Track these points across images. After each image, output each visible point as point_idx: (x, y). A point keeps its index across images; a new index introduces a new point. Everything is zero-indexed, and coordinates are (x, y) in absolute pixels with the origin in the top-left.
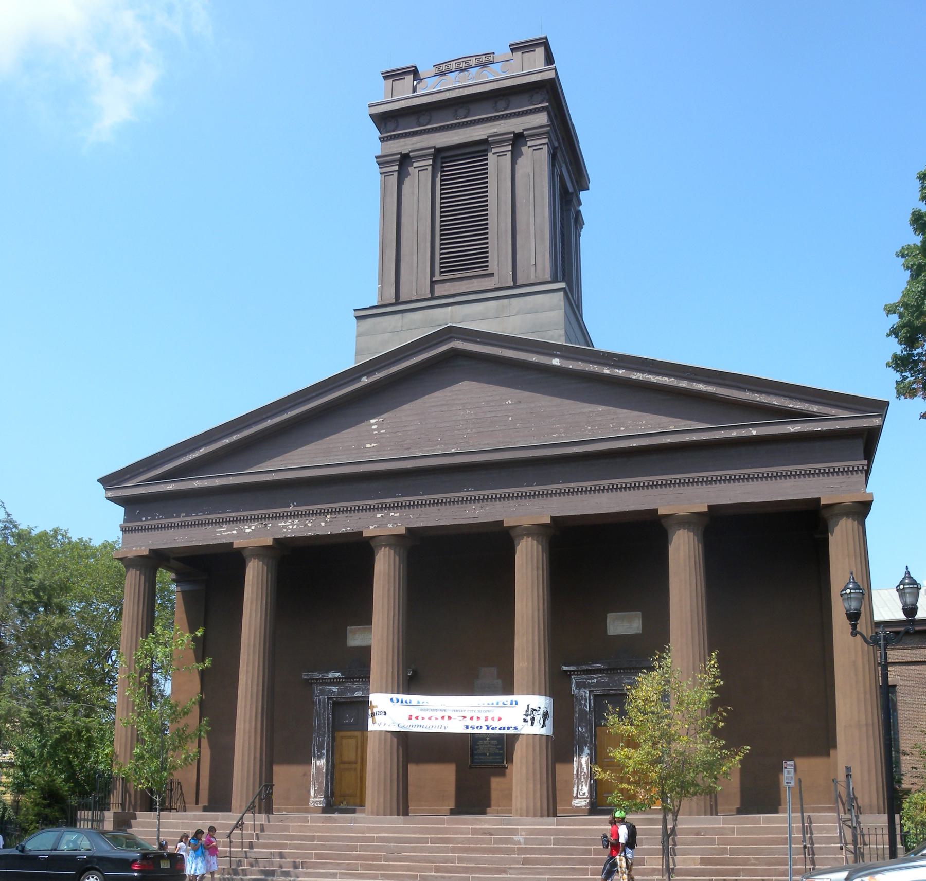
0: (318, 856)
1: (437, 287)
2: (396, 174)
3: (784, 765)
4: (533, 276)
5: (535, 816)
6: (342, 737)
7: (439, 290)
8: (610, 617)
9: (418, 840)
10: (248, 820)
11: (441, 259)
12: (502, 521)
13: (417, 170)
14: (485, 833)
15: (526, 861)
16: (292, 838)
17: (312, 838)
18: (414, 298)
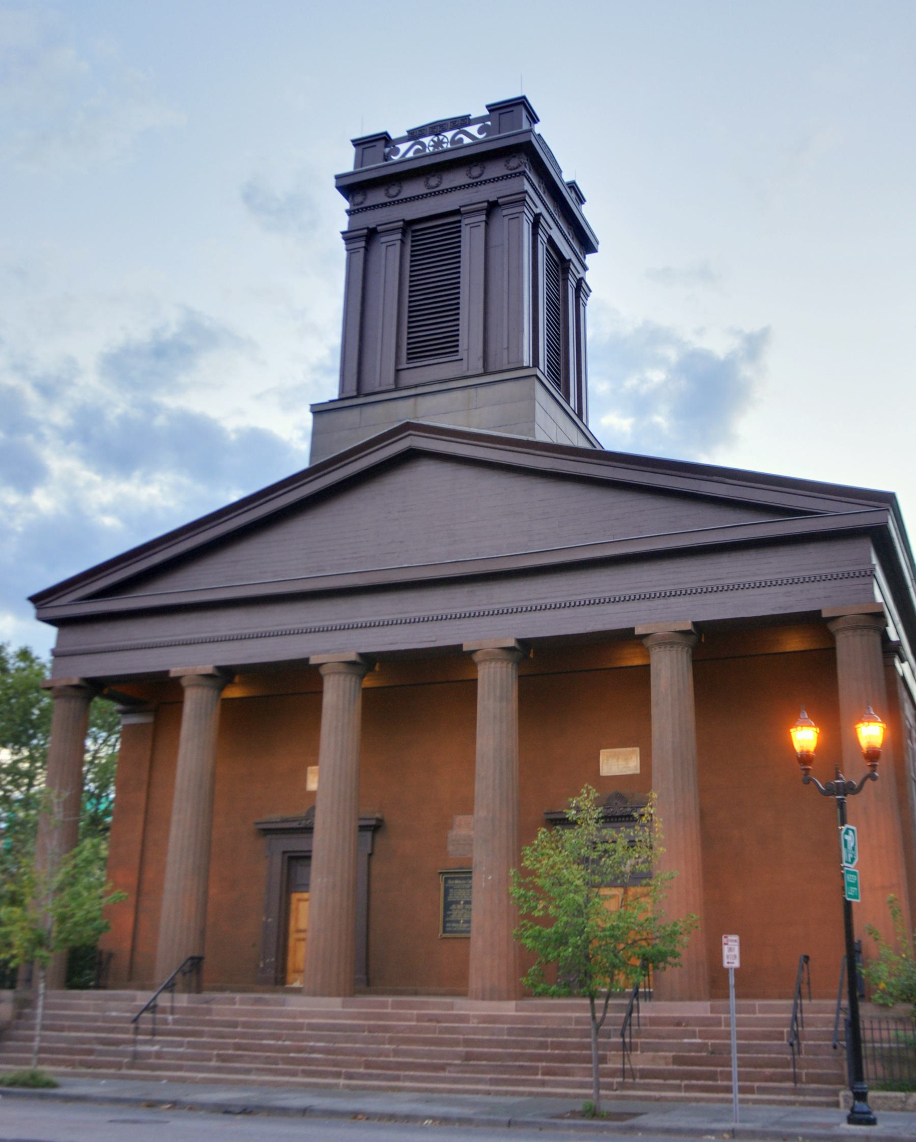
0: (238, 1047)
1: (403, 374)
2: (362, 250)
3: (724, 940)
4: (505, 361)
5: (483, 999)
6: (299, 900)
7: (408, 378)
8: (604, 754)
9: (353, 1028)
10: (164, 1000)
11: (409, 344)
12: (461, 646)
13: (468, 227)
14: (430, 1020)
15: (468, 1057)
16: (212, 1023)
17: (234, 1024)
18: (505, 368)
